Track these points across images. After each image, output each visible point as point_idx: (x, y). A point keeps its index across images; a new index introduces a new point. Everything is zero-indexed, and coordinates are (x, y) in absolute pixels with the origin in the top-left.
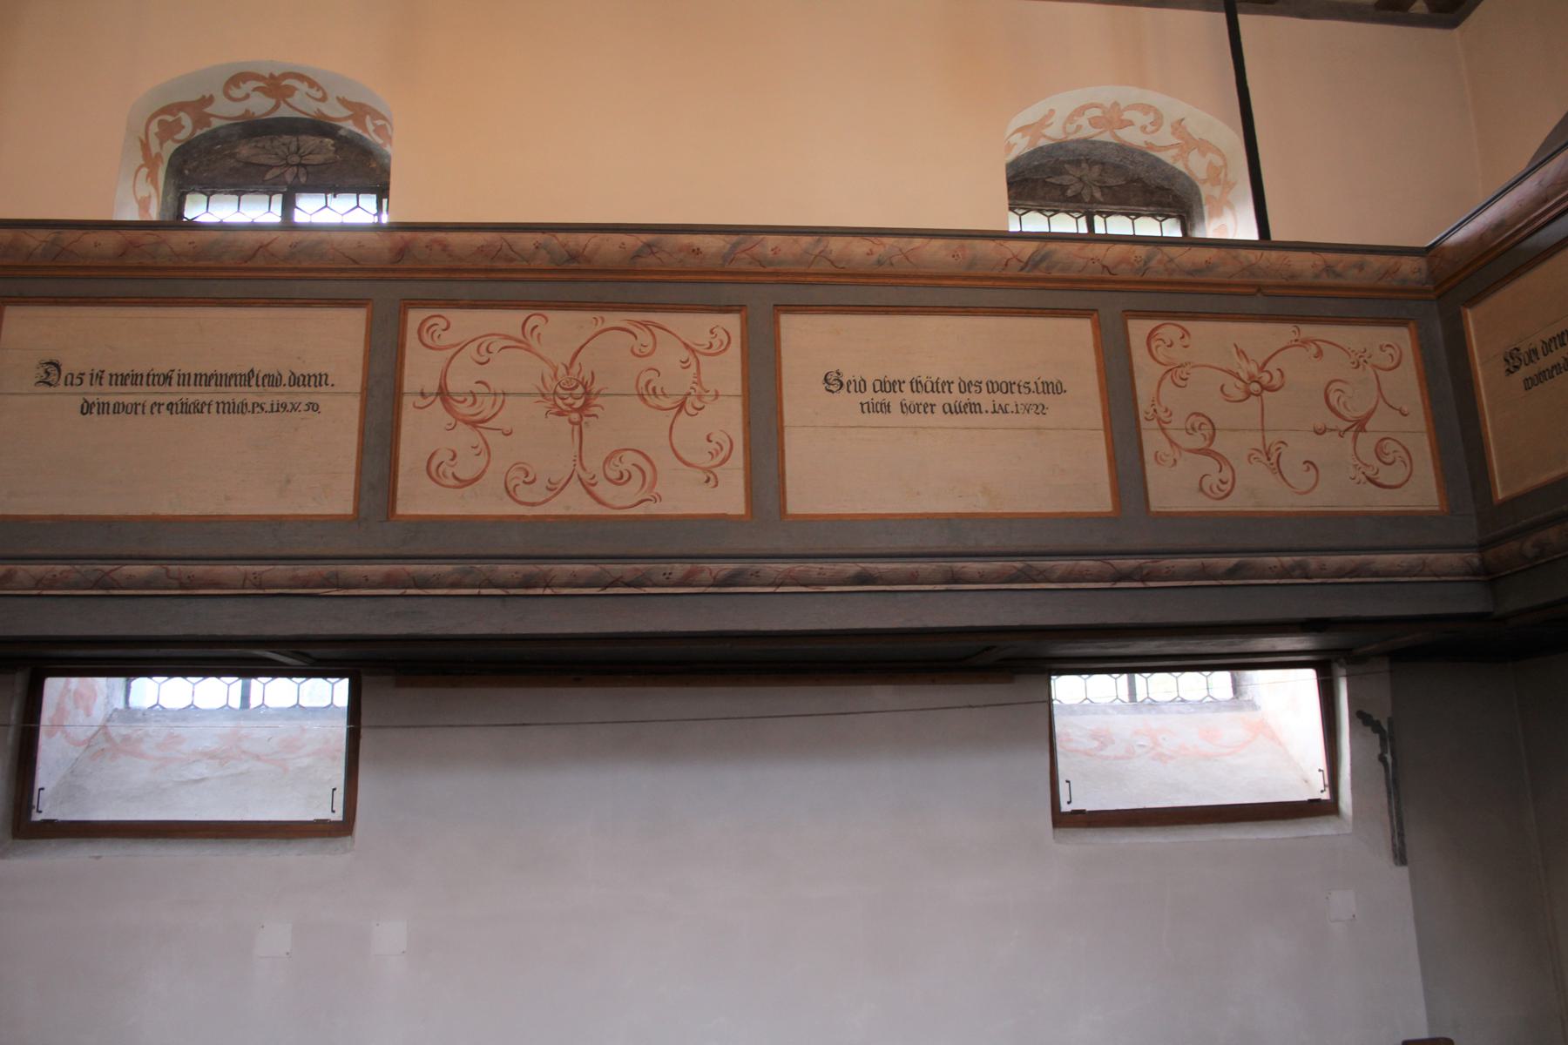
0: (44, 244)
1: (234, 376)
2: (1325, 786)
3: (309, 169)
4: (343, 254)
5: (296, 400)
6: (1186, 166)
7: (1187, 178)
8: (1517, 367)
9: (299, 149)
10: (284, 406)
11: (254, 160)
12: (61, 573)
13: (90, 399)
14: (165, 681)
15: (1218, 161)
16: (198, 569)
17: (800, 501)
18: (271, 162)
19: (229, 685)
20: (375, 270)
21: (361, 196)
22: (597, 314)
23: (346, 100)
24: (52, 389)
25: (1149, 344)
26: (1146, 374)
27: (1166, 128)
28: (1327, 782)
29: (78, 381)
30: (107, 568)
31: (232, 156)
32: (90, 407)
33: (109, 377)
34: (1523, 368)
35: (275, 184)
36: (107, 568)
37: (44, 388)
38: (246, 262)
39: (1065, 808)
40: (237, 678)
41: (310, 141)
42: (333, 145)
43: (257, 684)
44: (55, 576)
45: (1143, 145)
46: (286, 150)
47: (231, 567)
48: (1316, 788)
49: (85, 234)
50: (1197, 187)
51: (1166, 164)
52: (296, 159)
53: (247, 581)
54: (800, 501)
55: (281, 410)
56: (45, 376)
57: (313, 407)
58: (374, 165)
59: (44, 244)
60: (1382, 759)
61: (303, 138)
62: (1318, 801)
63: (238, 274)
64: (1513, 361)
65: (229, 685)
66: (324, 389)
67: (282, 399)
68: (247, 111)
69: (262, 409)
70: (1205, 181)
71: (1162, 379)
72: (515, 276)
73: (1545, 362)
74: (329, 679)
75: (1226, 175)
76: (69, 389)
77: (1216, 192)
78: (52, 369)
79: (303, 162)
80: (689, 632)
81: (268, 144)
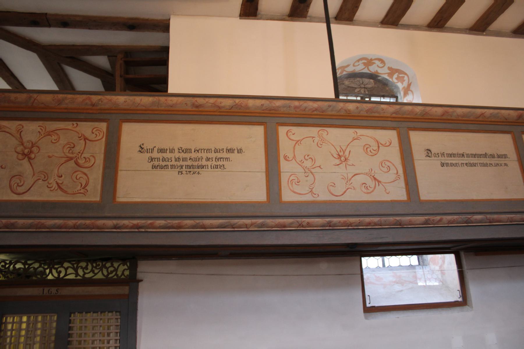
0: (421, 111)
1: (481, 155)
2: (460, 296)
3: (368, 89)
4: (504, 117)
5: (501, 162)
9: (363, 83)
10: (498, 164)
11: (350, 86)
12: (456, 219)
13: (443, 162)
14: (411, 257)
16: (495, 216)
17: (287, 196)
18: (356, 86)
19: (367, 260)
20: (512, 122)
21: (391, 98)
24: (430, 158)
28: (461, 295)
29: (438, 156)
30: (469, 217)
31: (343, 84)
32: (443, 164)
33: (446, 155)
35: (358, 94)
36: (469, 217)
37: (428, 158)
38: (477, 118)
39: (368, 305)
40: (380, 257)
41: (366, 80)
42: (373, 82)
43: (386, 258)
44: (454, 220)
46: (359, 83)
47: (504, 216)
49: (433, 108)
52: (363, 86)
53: (509, 220)
54: (287, 196)
55: (498, 165)
56: (427, 154)
57: (506, 165)
58: (387, 89)
59: (421, 111)
61: (364, 79)
62: (457, 301)
63: (417, 120)
65: (367, 260)
66: (507, 159)
67: (497, 162)
68: (354, 70)
69: (492, 165)
72: (499, 123)
74: (408, 256)
76: (436, 158)
78: (429, 152)
79: (365, 87)
80: (492, 238)
81: (353, 81)
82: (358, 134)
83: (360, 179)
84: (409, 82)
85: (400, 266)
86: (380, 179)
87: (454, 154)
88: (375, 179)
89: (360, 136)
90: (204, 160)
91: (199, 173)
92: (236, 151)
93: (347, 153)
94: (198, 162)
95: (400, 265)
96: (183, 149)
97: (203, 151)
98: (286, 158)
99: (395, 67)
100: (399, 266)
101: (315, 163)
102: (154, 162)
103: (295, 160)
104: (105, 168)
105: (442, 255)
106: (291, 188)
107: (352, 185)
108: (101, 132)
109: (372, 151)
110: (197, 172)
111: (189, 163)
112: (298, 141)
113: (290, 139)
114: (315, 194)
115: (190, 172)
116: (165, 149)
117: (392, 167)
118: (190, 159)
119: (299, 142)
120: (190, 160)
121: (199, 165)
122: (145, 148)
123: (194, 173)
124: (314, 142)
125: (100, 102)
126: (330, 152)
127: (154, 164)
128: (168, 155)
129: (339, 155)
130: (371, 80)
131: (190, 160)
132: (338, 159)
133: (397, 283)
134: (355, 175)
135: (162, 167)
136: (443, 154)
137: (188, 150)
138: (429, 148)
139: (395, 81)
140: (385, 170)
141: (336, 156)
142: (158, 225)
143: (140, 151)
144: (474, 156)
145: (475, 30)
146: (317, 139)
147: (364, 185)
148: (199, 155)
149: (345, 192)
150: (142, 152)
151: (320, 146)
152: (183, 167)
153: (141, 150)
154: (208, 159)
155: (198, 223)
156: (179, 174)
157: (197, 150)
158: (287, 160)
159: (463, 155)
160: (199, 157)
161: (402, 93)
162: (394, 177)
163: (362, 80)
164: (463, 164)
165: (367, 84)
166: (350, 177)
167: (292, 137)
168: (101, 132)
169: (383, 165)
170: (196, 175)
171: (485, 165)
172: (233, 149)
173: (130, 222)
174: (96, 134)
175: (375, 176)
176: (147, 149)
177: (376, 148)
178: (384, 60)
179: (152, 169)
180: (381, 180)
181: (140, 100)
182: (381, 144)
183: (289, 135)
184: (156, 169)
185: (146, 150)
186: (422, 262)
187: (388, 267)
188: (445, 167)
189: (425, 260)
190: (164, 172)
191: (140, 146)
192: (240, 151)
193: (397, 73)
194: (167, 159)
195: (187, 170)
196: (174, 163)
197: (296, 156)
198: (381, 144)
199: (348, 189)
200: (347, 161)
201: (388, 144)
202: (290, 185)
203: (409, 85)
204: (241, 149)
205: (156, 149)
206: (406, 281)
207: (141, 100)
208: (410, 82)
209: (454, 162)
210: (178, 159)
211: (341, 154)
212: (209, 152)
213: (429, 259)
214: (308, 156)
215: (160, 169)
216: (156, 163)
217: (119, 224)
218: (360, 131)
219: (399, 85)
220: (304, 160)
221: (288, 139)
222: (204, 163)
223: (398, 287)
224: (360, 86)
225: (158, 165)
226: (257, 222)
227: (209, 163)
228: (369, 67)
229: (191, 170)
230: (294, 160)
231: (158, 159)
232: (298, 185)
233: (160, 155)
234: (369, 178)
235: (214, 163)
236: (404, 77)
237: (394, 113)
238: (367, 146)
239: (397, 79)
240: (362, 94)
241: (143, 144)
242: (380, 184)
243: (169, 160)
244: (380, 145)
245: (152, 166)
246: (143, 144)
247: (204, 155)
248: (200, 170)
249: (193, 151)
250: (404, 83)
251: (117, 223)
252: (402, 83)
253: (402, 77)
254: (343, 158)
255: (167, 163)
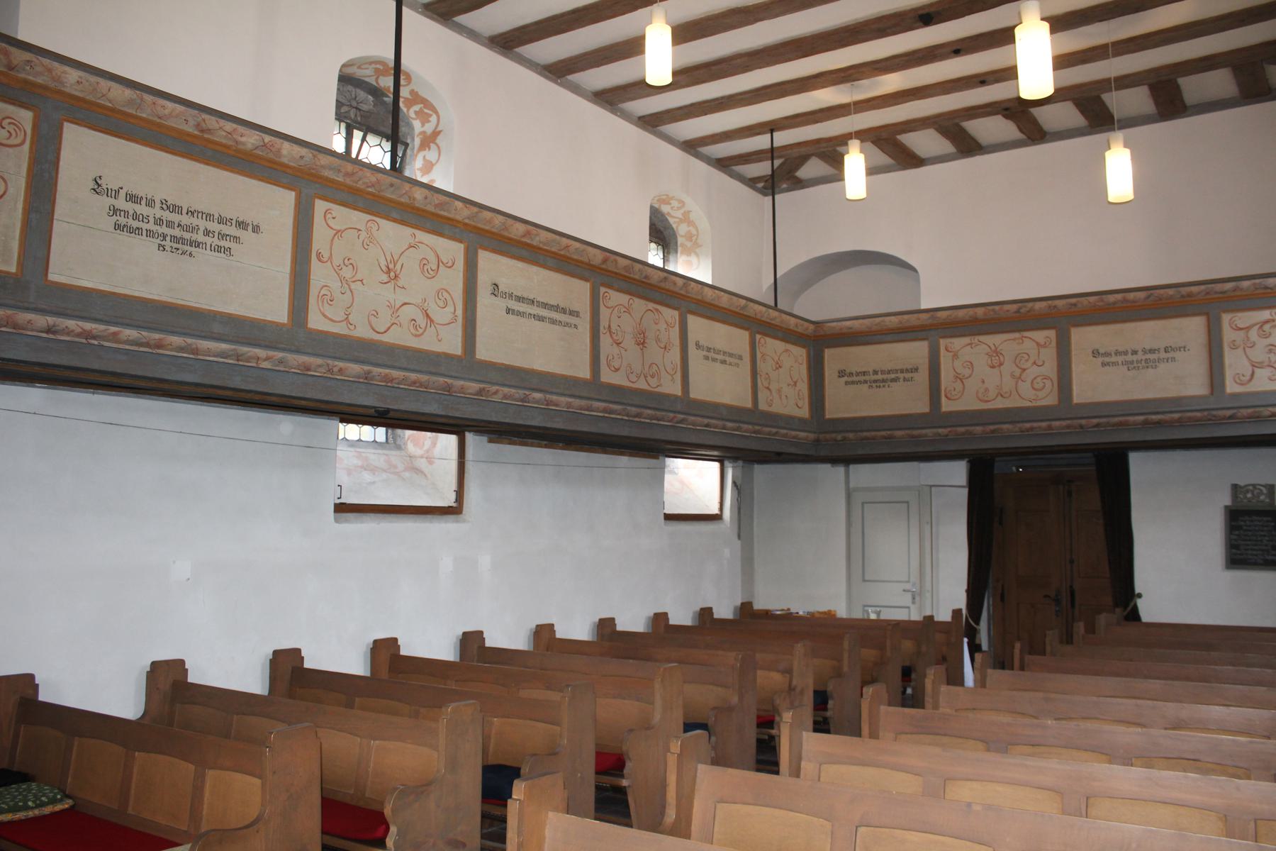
6: (677, 227)
7: (674, 231)
8: (843, 376)
9: (356, 97)
15: (694, 232)
22: (647, 303)
23: (418, 95)
25: (325, 217)
26: (320, 236)
27: (682, 211)
30: (527, 393)
34: (846, 377)
36: (527, 393)
39: (1141, 467)
41: (362, 94)
45: (666, 212)
48: (714, 510)
50: (676, 237)
51: (669, 223)
52: (354, 104)
57: (576, 326)
60: (738, 500)
64: (842, 374)
70: (682, 236)
71: (333, 238)
73: (855, 378)
75: (696, 239)
77: (689, 244)
82: (417, 240)
83: (409, 312)
84: (436, 128)
85: (360, 440)
86: (433, 318)
87: (523, 298)
88: (427, 315)
89: (419, 243)
90: (201, 232)
91: (191, 254)
92: (250, 228)
93: (398, 266)
94: (191, 234)
95: (345, 438)
96: (168, 204)
97: (200, 215)
98: (319, 255)
99: (423, 93)
100: (358, 440)
101: (356, 273)
102: (118, 218)
103: (332, 263)
104: (28, 211)
105: (434, 434)
106: (322, 309)
107: (398, 318)
108: (20, 129)
109: (429, 270)
110: (188, 253)
111: (177, 232)
112: (339, 231)
113: (327, 224)
114: (351, 325)
115: (178, 249)
116: (139, 196)
117: (450, 302)
118: (179, 225)
119: (340, 233)
120: (178, 227)
121: (192, 239)
122: (104, 187)
123: (184, 253)
124: (359, 238)
125: (28, 68)
126: (378, 260)
127: (118, 220)
128: (142, 209)
129: (388, 267)
130: (370, 97)
131: (178, 227)
132: (387, 273)
133: (365, 469)
134: (403, 305)
135: (132, 231)
136: (511, 296)
137: (177, 208)
138: (497, 282)
139: (412, 114)
140: (441, 304)
141: (384, 268)
142: (126, 338)
143: (94, 189)
144: (545, 306)
145: (550, 72)
146: (363, 235)
147: (413, 322)
148: (195, 221)
149: (389, 328)
150: (97, 193)
151: (366, 247)
152: (167, 239)
153: (96, 187)
154: (207, 233)
155: (190, 345)
156: (159, 250)
157: (191, 211)
158: (320, 260)
159: (533, 302)
160: (194, 225)
161: (417, 141)
162: (448, 318)
163: (356, 92)
164: (531, 315)
165: (361, 103)
166: (397, 306)
167: (331, 222)
168: (20, 129)
169: (440, 297)
170: (186, 257)
171: (553, 322)
172: (139, 196)
173: (78, 325)
174: (9, 132)
175: (428, 312)
176: (107, 189)
177: (435, 267)
178: (413, 76)
179: (114, 231)
180: (435, 320)
181: (108, 88)
182: (443, 263)
183: (327, 218)
184: (121, 232)
185: (106, 190)
186: (393, 438)
187: (343, 439)
188: (510, 316)
189: (400, 437)
190: (135, 240)
191: (95, 180)
192: (256, 229)
193: (422, 105)
194: (141, 216)
195: (172, 244)
196: (151, 226)
197: (333, 256)
198: (443, 263)
199: (393, 324)
200: (397, 280)
201: (450, 264)
202: (320, 304)
203: (436, 134)
204: (258, 226)
205: (122, 193)
206: (376, 467)
207: (109, 90)
208: (439, 129)
209: (521, 310)
210: (159, 222)
211: (391, 266)
212: (210, 220)
213: (406, 437)
214: (348, 260)
215: (128, 234)
216: (122, 221)
217: (58, 326)
218: (422, 236)
219: (417, 125)
220: (342, 266)
221: (325, 225)
222: (200, 237)
223: (367, 476)
224: (350, 101)
225: (125, 225)
226: (274, 356)
227: (208, 240)
228: (381, 77)
229: (179, 246)
230: (329, 262)
231: (127, 213)
232: (331, 305)
233: (129, 207)
234: (420, 311)
235: (216, 241)
236: (431, 115)
237: (468, 218)
238: (425, 262)
239: (416, 112)
240: (350, 119)
241: (100, 177)
242: (432, 325)
243: (145, 219)
244: (441, 264)
245: (115, 223)
246: (100, 177)
247: (203, 224)
248: (193, 249)
249: (185, 211)
250: (427, 125)
251: (55, 323)
252: (423, 125)
253: (426, 113)
254: (392, 274)
255: (140, 225)
